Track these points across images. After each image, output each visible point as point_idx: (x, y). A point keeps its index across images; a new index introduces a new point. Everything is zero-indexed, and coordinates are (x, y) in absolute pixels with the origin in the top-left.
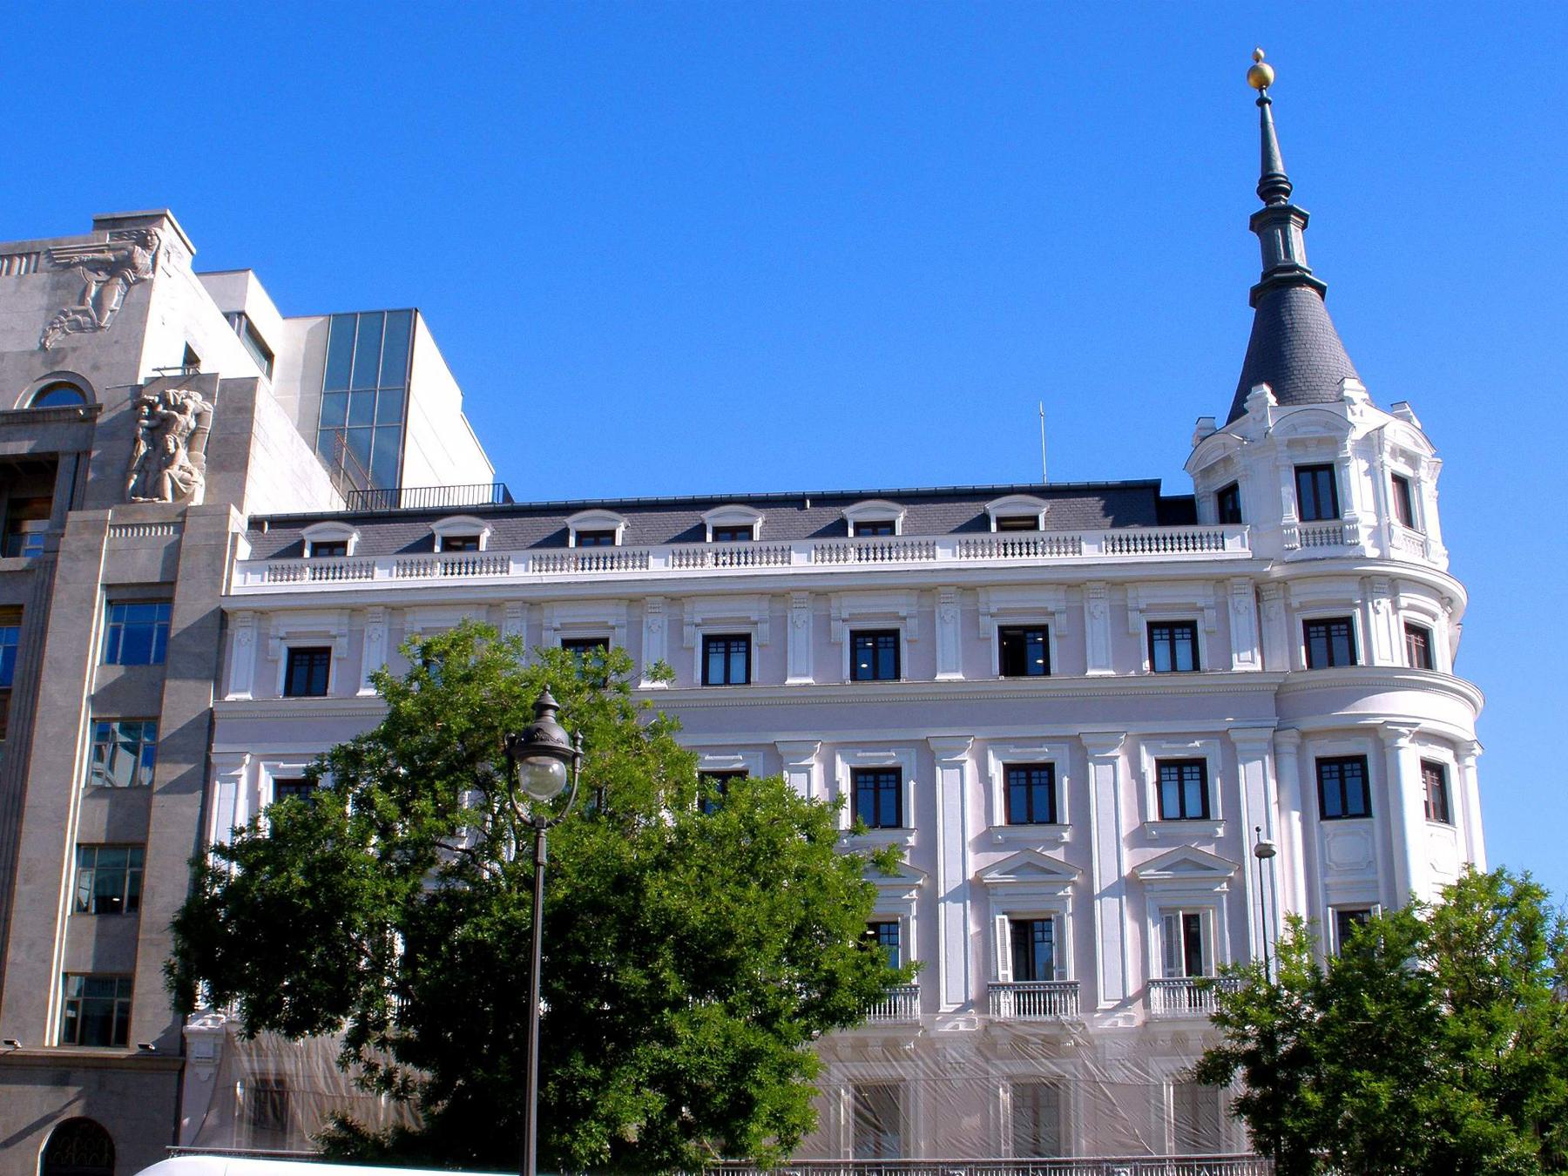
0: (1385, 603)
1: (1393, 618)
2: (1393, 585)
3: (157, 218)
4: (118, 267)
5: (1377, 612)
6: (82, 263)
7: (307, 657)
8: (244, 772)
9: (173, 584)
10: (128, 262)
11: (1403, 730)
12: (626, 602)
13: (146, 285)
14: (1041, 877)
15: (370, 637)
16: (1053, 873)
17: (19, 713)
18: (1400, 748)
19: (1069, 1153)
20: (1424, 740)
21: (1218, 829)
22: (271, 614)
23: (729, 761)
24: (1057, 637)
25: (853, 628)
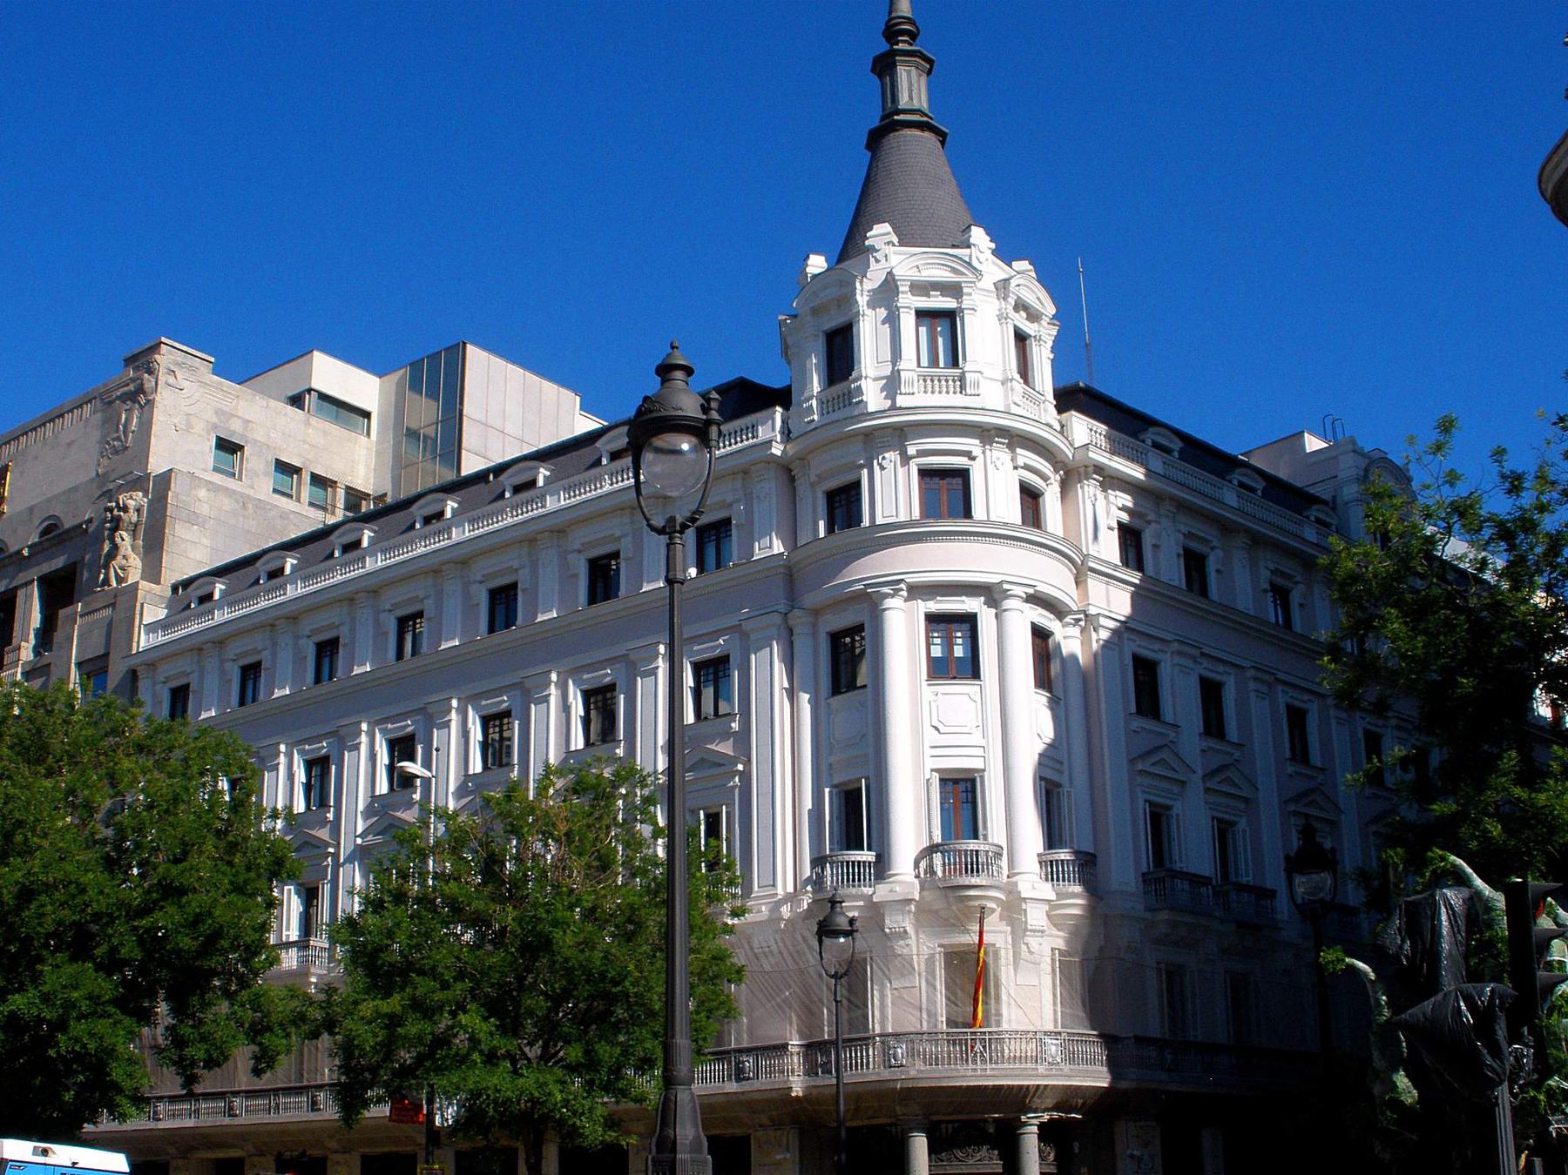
0: (892, 456)
1: (901, 471)
2: (898, 436)
3: (155, 348)
4: (132, 397)
5: (882, 468)
6: (118, 398)
7: (843, 496)
8: (364, 738)
9: (108, 653)
10: (141, 390)
11: (886, 590)
12: (861, 437)
13: (150, 403)
14: (715, 771)
15: (758, 497)
16: (720, 765)
17: (358, 684)
18: (885, 610)
19: (998, 1023)
20: (929, 594)
21: (328, 815)
22: (809, 457)
23: (498, 702)
24: (523, 591)
25: (317, 641)
